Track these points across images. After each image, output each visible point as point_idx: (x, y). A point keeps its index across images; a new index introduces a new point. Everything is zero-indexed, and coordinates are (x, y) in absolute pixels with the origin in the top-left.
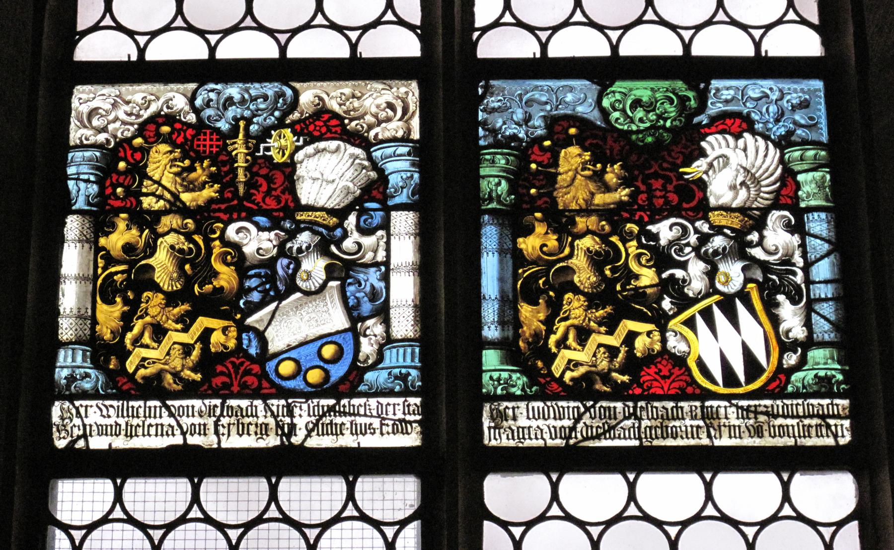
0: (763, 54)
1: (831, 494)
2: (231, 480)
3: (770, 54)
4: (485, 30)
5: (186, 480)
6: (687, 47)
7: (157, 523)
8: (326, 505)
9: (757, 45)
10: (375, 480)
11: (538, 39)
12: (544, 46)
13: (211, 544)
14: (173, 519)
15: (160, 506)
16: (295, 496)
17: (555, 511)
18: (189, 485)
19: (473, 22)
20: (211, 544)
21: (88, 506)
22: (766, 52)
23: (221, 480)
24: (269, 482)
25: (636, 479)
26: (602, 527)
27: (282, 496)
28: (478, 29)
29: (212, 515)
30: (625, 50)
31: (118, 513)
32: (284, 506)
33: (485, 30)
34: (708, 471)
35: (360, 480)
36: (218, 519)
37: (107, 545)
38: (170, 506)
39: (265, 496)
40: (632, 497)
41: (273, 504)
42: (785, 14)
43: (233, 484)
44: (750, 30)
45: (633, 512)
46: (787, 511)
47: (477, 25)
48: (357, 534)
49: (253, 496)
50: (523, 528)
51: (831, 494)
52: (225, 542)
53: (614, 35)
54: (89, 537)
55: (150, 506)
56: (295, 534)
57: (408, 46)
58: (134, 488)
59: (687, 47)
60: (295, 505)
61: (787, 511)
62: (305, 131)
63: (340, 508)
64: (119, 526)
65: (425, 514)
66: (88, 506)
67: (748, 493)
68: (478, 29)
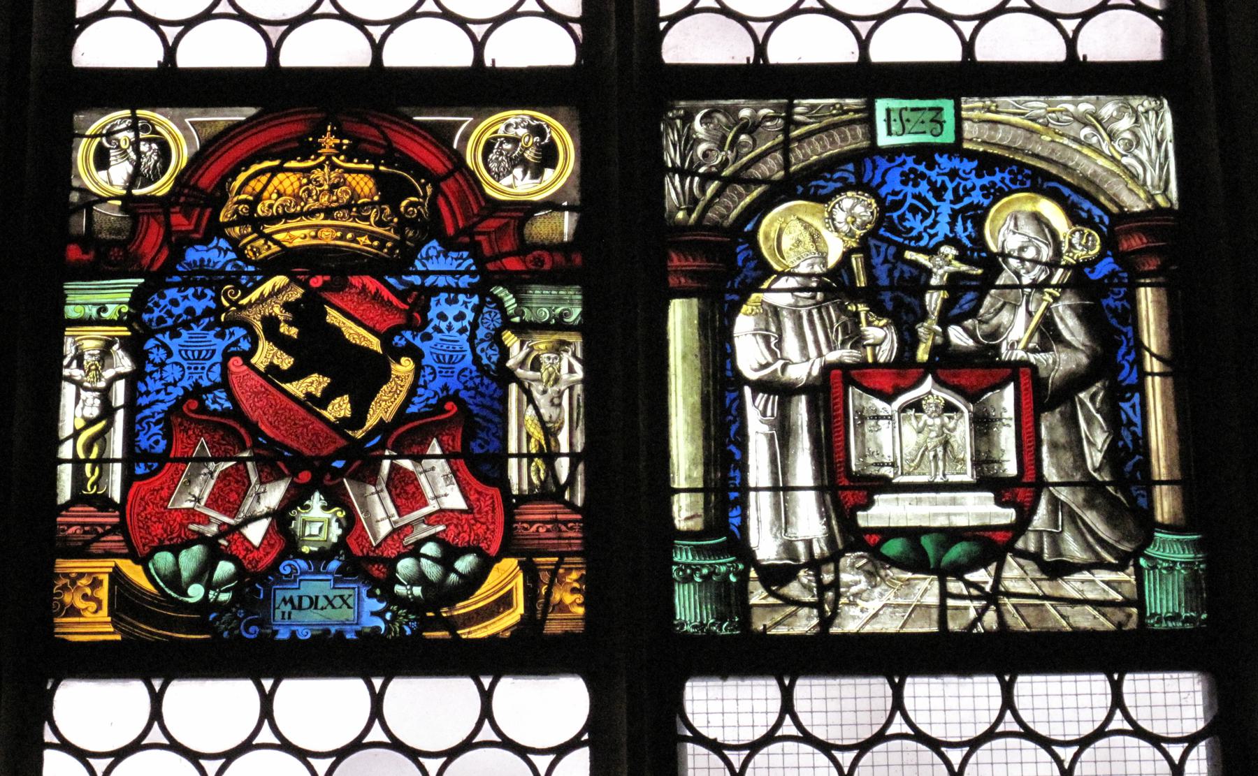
0: (488, 63)
1: (1174, 700)
2: (1153, 676)
3: (1089, 59)
4: (673, 19)
5: (1103, 677)
6: (968, 47)
7: (846, 743)
8: (864, 718)
9: (1071, 43)
10: (710, 683)
11: (1062, 31)
12: (377, 48)
13: (1148, 768)
14: (868, 736)
15: (849, 718)
16: (1040, 702)
17: (156, 736)
18: (888, 686)
19: (657, 11)
20: (1148, 768)
21: (746, 719)
22: (493, 61)
23: (815, 681)
24: (781, 684)
25: (493, 685)
26: (532, 757)
27: (800, 705)
28: (663, 19)
29: (925, 729)
30: (983, 53)
31: (1009, 724)
32: (804, 719)
33: (673, 19)
34: (486, 674)
35: (909, 680)
36: (1155, 732)
37: (1103, 768)
38: (1085, 714)
39: (776, 705)
40: (486, 712)
41: (788, 717)
42: (1076, 756)
43: (950, 686)
44: (956, 22)
45: (487, 734)
46: (487, 734)
47: (662, 14)
48: (1014, 756)
49: (760, 706)
50: (92, 761)
51: (1174, 700)
52: (1166, 763)
53: (967, 28)
54: (751, 765)
55: (1056, 715)
56: (1043, 754)
57: (557, 49)
58: (918, 689)
59: (968, 47)
60: (1041, 715)
61: (1120, 723)
62: (1015, 168)
63: (884, 721)
64: (790, 745)
65: (597, 734)
66: (746, 719)
67: (1063, 700)
68: (663, 19)
